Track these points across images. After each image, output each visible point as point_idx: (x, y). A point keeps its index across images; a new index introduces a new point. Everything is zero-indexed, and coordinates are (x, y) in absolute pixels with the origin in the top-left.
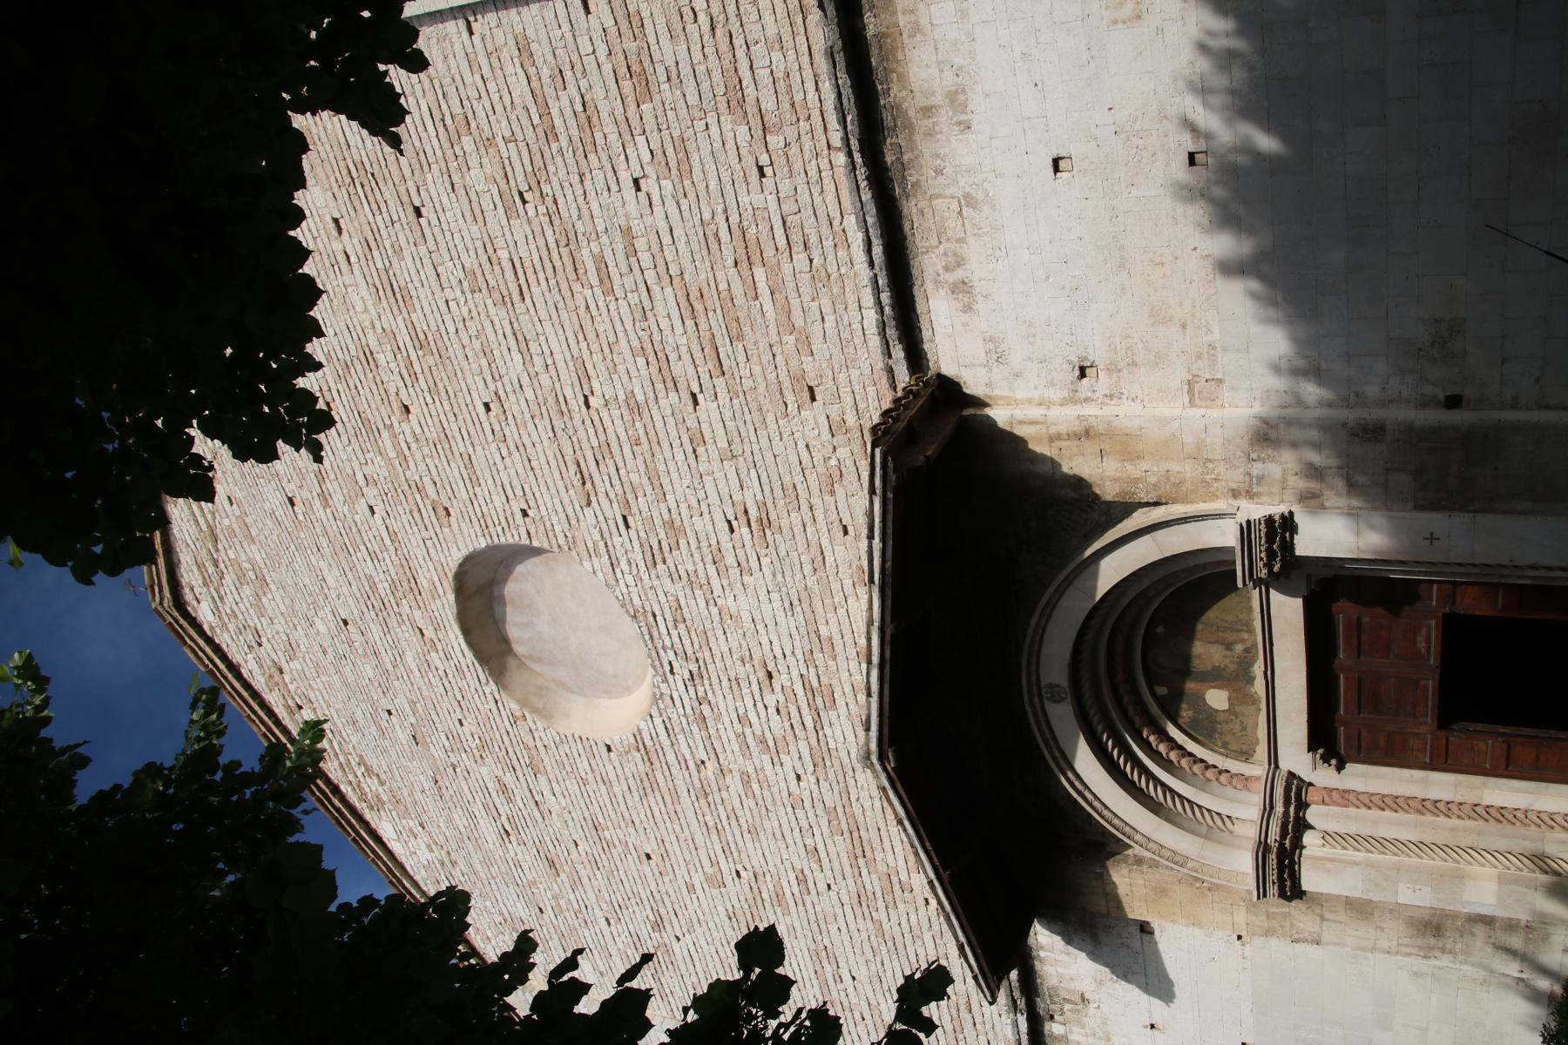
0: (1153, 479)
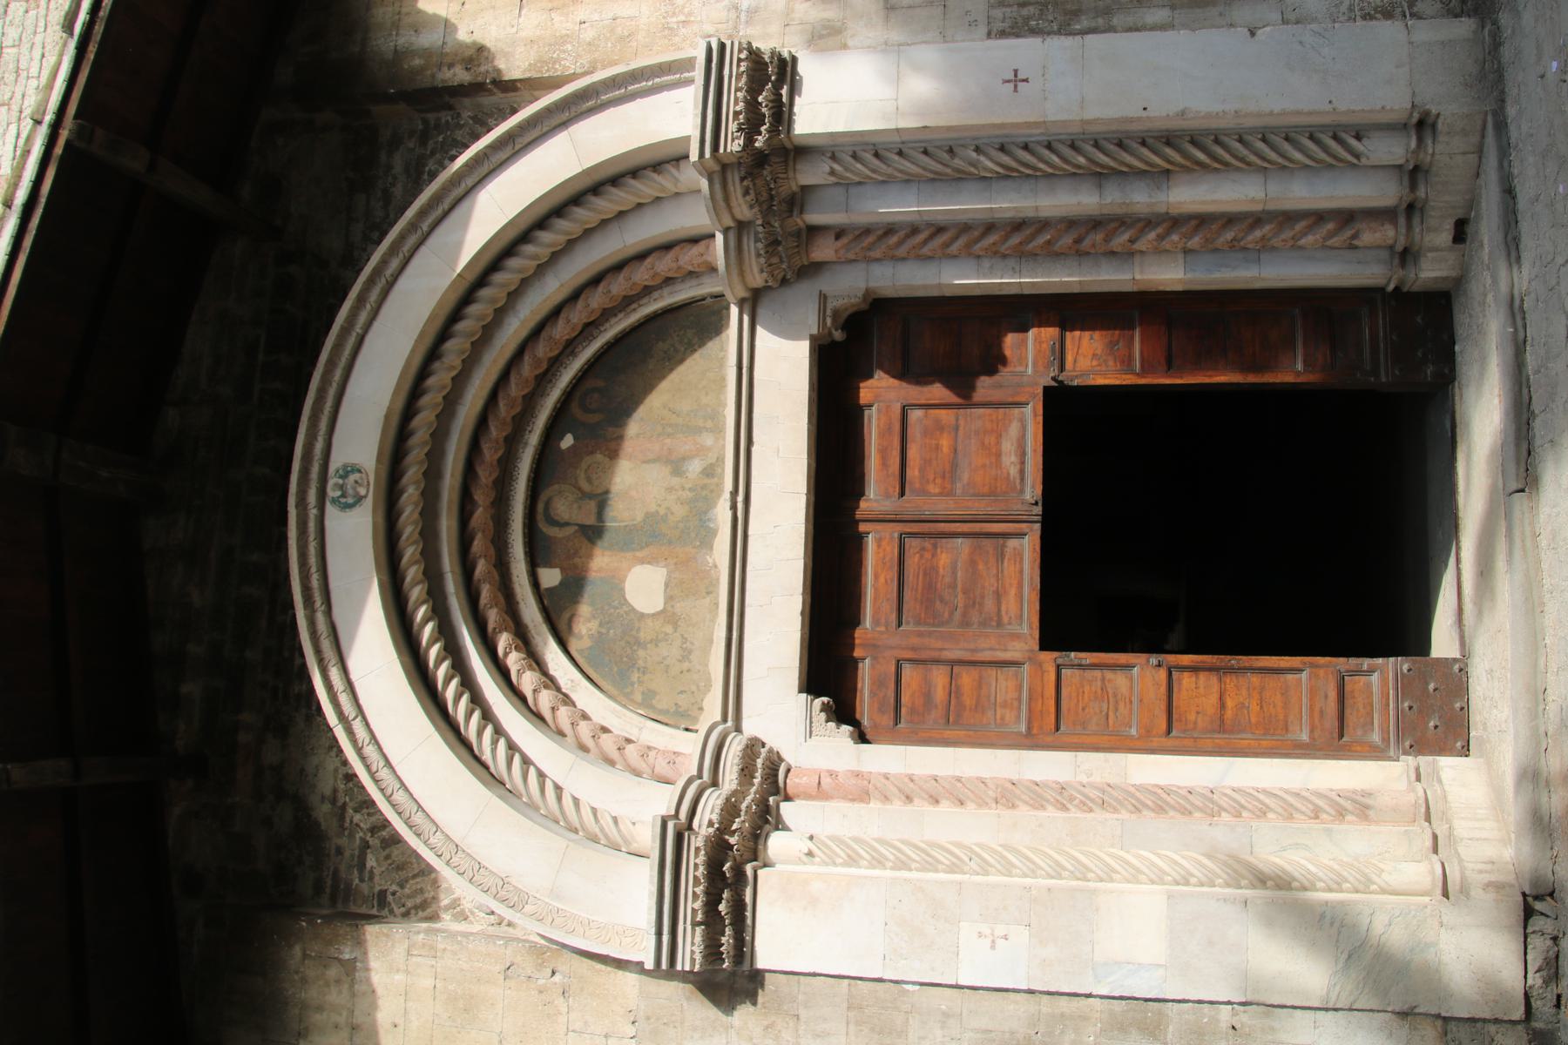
0: (588, 34)
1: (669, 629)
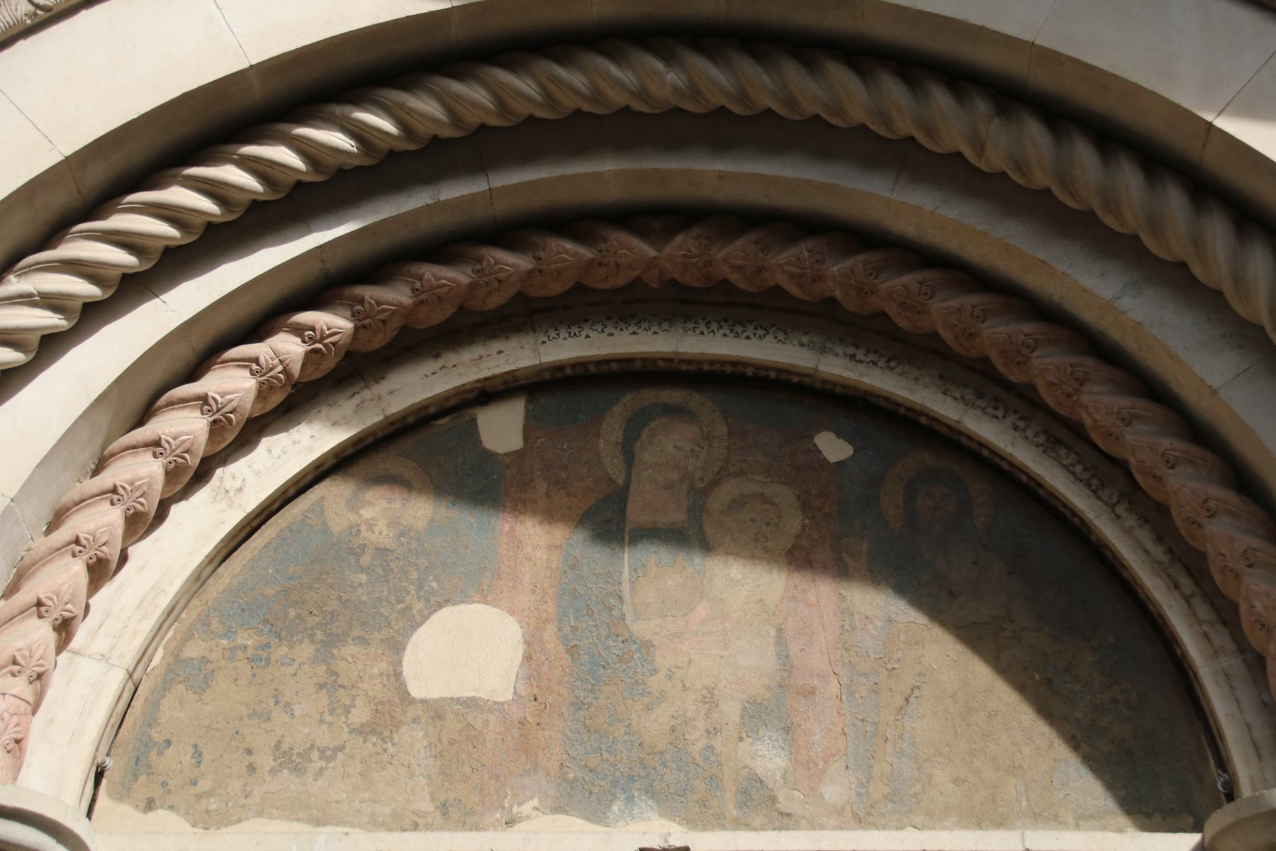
1: (360, 714)
